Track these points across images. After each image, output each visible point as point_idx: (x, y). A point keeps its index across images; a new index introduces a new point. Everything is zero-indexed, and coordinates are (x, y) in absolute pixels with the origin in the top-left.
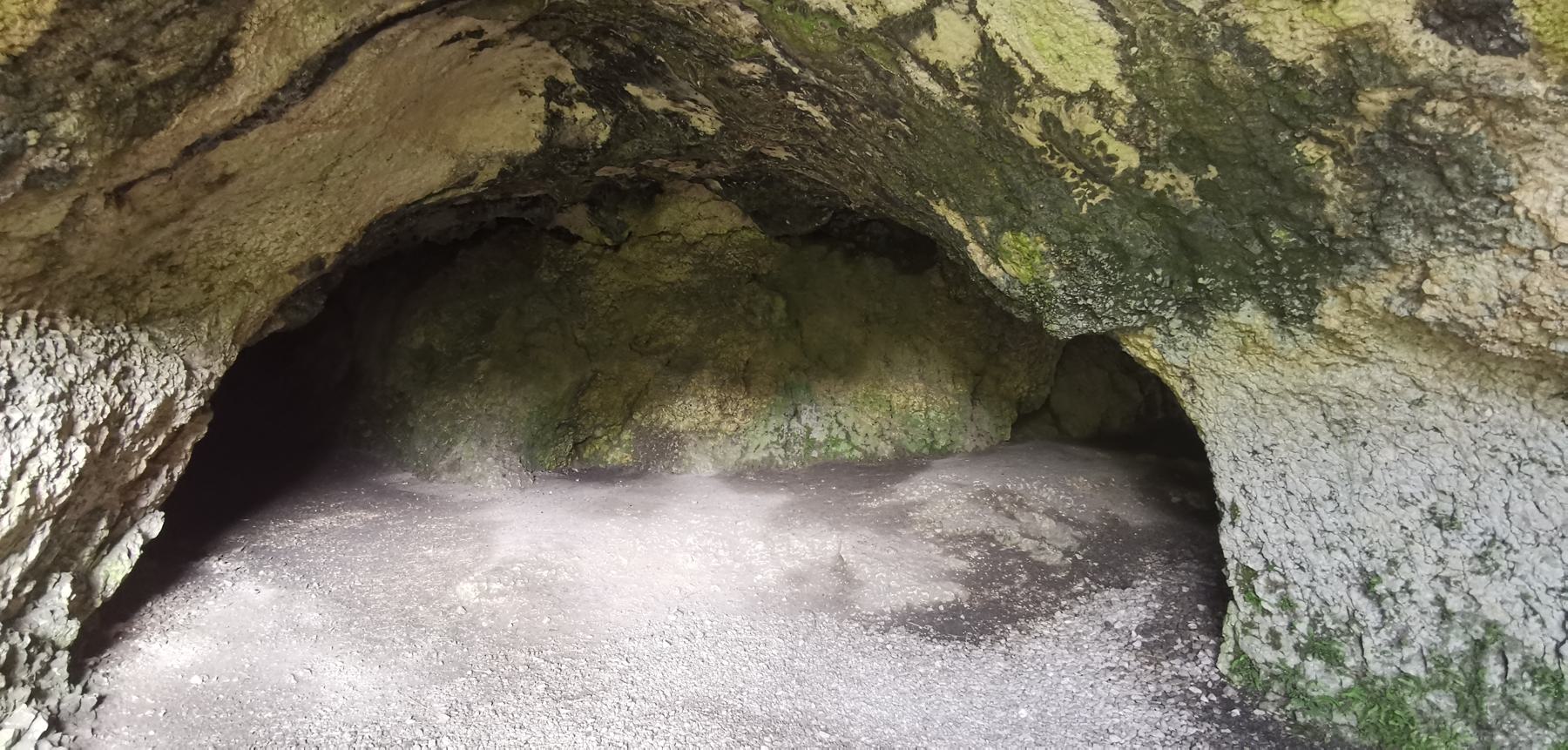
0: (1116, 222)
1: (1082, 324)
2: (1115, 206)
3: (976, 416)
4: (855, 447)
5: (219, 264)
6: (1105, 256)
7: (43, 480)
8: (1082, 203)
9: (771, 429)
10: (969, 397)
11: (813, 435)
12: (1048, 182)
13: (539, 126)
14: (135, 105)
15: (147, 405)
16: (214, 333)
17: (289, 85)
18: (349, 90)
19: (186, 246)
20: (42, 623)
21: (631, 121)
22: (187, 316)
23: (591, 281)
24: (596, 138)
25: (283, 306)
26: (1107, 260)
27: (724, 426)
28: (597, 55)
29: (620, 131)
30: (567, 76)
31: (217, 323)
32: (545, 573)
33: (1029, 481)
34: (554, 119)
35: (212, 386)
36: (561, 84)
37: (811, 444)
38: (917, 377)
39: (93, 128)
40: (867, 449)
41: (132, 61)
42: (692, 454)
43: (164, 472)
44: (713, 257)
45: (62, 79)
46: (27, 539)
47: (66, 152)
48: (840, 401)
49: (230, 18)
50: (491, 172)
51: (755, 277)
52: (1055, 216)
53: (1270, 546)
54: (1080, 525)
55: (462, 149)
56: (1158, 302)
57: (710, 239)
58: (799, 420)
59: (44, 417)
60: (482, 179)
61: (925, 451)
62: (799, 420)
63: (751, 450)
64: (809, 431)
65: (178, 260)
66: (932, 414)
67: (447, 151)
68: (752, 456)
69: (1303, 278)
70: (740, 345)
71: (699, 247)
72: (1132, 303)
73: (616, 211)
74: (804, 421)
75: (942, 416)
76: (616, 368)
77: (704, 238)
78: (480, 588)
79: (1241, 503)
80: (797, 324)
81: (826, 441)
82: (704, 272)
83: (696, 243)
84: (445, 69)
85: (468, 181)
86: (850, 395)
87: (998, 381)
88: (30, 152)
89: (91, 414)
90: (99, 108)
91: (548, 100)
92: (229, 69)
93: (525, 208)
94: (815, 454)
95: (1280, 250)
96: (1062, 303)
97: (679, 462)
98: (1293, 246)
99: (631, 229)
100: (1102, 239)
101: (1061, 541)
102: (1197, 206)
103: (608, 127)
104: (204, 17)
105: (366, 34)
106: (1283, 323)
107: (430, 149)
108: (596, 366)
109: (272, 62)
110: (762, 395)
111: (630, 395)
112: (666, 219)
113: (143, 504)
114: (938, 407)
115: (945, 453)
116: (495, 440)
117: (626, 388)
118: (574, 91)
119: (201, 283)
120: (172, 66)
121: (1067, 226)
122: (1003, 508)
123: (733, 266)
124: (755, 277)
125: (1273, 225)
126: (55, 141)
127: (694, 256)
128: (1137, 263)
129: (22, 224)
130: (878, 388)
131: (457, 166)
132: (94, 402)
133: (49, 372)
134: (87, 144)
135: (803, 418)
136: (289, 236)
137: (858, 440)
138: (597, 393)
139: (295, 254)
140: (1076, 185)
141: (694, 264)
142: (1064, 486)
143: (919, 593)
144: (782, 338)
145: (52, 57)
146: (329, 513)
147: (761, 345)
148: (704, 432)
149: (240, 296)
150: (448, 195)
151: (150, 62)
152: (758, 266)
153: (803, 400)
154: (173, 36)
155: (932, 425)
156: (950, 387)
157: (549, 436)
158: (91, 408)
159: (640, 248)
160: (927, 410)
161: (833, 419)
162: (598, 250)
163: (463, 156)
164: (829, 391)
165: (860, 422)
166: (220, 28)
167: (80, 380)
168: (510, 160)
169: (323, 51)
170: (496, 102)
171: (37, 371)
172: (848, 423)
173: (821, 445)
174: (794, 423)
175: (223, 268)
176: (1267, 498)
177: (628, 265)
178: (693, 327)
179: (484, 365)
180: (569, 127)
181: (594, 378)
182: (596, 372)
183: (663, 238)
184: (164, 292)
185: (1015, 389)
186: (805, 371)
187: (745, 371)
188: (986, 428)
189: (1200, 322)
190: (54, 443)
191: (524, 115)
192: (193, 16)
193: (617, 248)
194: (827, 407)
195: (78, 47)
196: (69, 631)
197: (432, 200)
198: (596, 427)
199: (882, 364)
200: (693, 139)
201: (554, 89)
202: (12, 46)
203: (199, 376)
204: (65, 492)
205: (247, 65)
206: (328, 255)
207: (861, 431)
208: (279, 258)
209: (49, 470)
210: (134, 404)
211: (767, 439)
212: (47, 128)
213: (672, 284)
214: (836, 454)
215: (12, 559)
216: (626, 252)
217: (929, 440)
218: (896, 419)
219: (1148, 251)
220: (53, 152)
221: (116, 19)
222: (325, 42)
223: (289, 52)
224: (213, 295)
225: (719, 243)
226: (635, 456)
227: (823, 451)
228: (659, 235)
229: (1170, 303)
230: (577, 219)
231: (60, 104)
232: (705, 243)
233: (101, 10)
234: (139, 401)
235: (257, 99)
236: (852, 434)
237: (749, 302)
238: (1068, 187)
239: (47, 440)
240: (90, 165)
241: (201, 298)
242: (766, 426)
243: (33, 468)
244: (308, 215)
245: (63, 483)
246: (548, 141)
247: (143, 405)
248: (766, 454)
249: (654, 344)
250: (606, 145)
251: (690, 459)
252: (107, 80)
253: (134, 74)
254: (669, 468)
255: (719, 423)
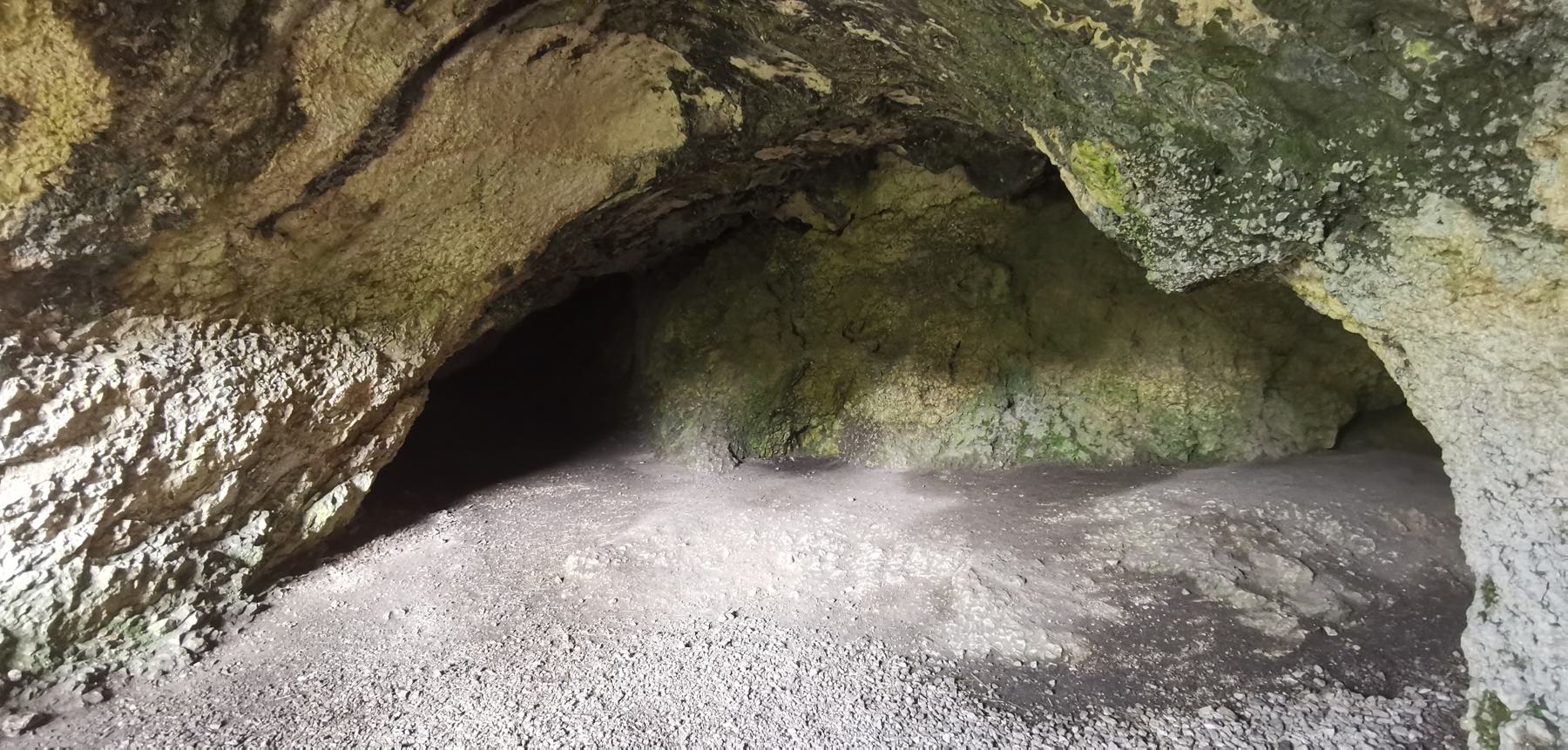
0: (1181, 94)
1: (1187, 268)
2: (1174, 69)
3: (1269, 413)
4: (1081, 447)
5: (414, 277)
6: (1180, 154)
7: (221, 443)
8: (1131, 75)
9: (978, 422)
10: (1260, 388)
11: (1029, 431)
12: (1077, 55)
13: (679, 120)
14: (225, 157)
15: (336, 385)
16: (414, 332)
17: (375, 120)
18: (445, 118)
19: (381, 266)
20: (233, 546)
21: (754, 95)
22: (389, 323)
23: (814, 268)
24: (733, 121)
25: (488, 309)
26: (1183, 160)
27: (925, 418)
28: (692, 36)
29: (751, 108)
30: (683, 65)
31: (417, 324)
32: (646, 556)
33: (1303, 507)
34: (688, 110)
35: (411, 375)
36: (682, 73)
37: (1025, 441)
38: (1175, 360)
39: (192, 178)
40: (1098, 451)
41: (208, 124)
42: (888, 448)
43: (373, 441)
44: (935, 230)
45: (150, 143)
46: (217, 484)
47: (172, 199)
48: (1067, 390)
49: (277, 74)
50: (649, 172)
51: (979, 249)
52: (1108, 106)
53: (1538, 670)
54: (1361, 581)
55: (615, 154)
56: (1281, 217)
57: (932, 212)
58: (1013, 414)
59: (219, 396)
60: (642, 180)
61: (1183, 456)
62: (1013, 414)
63: (952, 446)
64: (1025, 425)
65: (379, 276)
66: (1196, 408)
67: (598, 158)
68: (951, 453)
69: (1490, 129)
70: (949, 326)
71: (921, 222)
72: (1243, 225)
73: (831, 195)
74: (1018, 415)
75: (1211, 412)
76: (825, 356)
77: (927, 210)
78: (579, 562)
79: (1501, 579)
80: (1023, 299)
81: (1045, 439)
82: (923, 248)
83: (918, 217)
84: (551, 82)
85: (631, 183)
86: (1081, 382)
87: (1316, 362)
88: (144, 202)
89: (272, 394)
90: (194, 162)
91: (678, 93)
92: (301, 118)
93: (739, 203)
94: (1029, 453)
95: (1429, 82)
96: (1158, 237)
97: (872, 456)
98: (1444, 68)
99: (852, 211)
100: (1178, 128)
101: (1311, 603)
102: (1274, 33)
103: (739, 108)
104: (250, 76)
105: (433, 64)
106: (1495, 229)
107: (579, 159)
108: (807, 354)
109: (347, 105)
110: (968, 383)
111: (842, 384)
112: (883, 195)
113: (354, 464)
114: (1204, 399)
115: (1213, 461)
116: (713, 425)
117: (835, 377)
118: (695, 77)
119: (401, 293)
120: (245, 123)
121: (1126, 118)
122: (1233, 543)
123: (955, 238)
124: (979, 249)
125: (1398, 35)
126: (162, 192)
127: (916, 232)
128: (1244, 156)
129: (194, 256)
130: (1120, 374)
131: (614, 170)
132: (275, 388)
133: (236, 363)
134: (190, 190)
135: (1018, 409)
136: (470, 251)
137: (1085, 439)
138: (811, 382)
139: (480, 265)
140: (1114, 49)
141: (914, 241)
142: (1375, 522)
143: (1013, 639)
144: (1002, 316)
145: (131, 128)
146: (588, 481)
147: (974, 326)
148: (903, 424)
149: (436, 302)
150: (618, 199)
151: (222, 122)
152: (983, 235)
153: (1021, 390)
154: (232, 98)
155: (1195, 421)
156: (1228, 372)
157: (763, 424)
158: (272, 390)
159: (860, 230)
160: (1188, 404)
161: (1057, 412)
162: (823, 237)
163: (616, 160)
164: (1053, 378)
165: (1091, 417)
166: (272, 84)
167: (266, 369)
168: (663, 156)
169: (397, 88)
170: (634, 105)
171: (222, 363)
172: (1075, 418)
173: (1038, 444)
174: (1008, 416)
175: (418, 280)
176: (1541, 574)
177: (848, 249)
178: (905, 309)
179: (714, 355)
180: (704, 114)
181: (807, 366)
182: (809, 360)
183: (884, 216)
184: (368, 302)
185: (1352, 374)
186: (1029, 354)
187: (954, 355)
188: (1286, 429)
189: (1374, 244)
190: (231, 415)
191: (663, 112)
192: (239, 78)
193: (839, 233)
194: (1051, 398)
195: (148, 119)
196: (255, 555)
197: (604, 206)
198: (811, 416)
199: (1128, 344)
200: (812, 102)
201: (679, 81)
202: (95, 125)
203: (395, 367)
204: (246, 451)
205: (319, 110)
206: (515, 263)
207: (1091, 428)
208: (467, 269)
209: (227, 436)
210: (324, 387)
211: (973, 434)
212: (152, 184)
213: (892, 264)
214: (1056, 453)
215: (205, 497)
216: (847, 235)
217: (1189, 443)
218: (1143, 414)
219: (1246, 132)
220: (162, 200)
221: (167, 93)
222: (394, 80)
223: (361, 94)
224: (413, 302)
225: (942, 214)
226: (841, 447)
227: (1040, 450)
228: (881, 213)
229: (1305, 216)
230: (798, 205)
231: (158, 164)
232: (928, 216)
233: (152, 87)
234: (329, 386)
235: (348, 139)
236: (1079, 431)
237: (966, 278)
238: (1103, 55)
239: (224, 413)
240: (199, 206)
241: (403, 305)
242: (972, 419)
243: (210, 433)
244: (481, 230)
245: (241, 445)
246: (689, 130)
247: (333, 389)
248: (969, 452)
249: (867, 330)
250: (744, 125)
251: (885, 453)
252: (191, 141)
253: (212, 132)
254: (862, 462)
255: (920, 414)
